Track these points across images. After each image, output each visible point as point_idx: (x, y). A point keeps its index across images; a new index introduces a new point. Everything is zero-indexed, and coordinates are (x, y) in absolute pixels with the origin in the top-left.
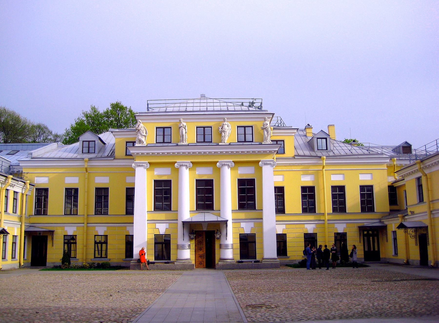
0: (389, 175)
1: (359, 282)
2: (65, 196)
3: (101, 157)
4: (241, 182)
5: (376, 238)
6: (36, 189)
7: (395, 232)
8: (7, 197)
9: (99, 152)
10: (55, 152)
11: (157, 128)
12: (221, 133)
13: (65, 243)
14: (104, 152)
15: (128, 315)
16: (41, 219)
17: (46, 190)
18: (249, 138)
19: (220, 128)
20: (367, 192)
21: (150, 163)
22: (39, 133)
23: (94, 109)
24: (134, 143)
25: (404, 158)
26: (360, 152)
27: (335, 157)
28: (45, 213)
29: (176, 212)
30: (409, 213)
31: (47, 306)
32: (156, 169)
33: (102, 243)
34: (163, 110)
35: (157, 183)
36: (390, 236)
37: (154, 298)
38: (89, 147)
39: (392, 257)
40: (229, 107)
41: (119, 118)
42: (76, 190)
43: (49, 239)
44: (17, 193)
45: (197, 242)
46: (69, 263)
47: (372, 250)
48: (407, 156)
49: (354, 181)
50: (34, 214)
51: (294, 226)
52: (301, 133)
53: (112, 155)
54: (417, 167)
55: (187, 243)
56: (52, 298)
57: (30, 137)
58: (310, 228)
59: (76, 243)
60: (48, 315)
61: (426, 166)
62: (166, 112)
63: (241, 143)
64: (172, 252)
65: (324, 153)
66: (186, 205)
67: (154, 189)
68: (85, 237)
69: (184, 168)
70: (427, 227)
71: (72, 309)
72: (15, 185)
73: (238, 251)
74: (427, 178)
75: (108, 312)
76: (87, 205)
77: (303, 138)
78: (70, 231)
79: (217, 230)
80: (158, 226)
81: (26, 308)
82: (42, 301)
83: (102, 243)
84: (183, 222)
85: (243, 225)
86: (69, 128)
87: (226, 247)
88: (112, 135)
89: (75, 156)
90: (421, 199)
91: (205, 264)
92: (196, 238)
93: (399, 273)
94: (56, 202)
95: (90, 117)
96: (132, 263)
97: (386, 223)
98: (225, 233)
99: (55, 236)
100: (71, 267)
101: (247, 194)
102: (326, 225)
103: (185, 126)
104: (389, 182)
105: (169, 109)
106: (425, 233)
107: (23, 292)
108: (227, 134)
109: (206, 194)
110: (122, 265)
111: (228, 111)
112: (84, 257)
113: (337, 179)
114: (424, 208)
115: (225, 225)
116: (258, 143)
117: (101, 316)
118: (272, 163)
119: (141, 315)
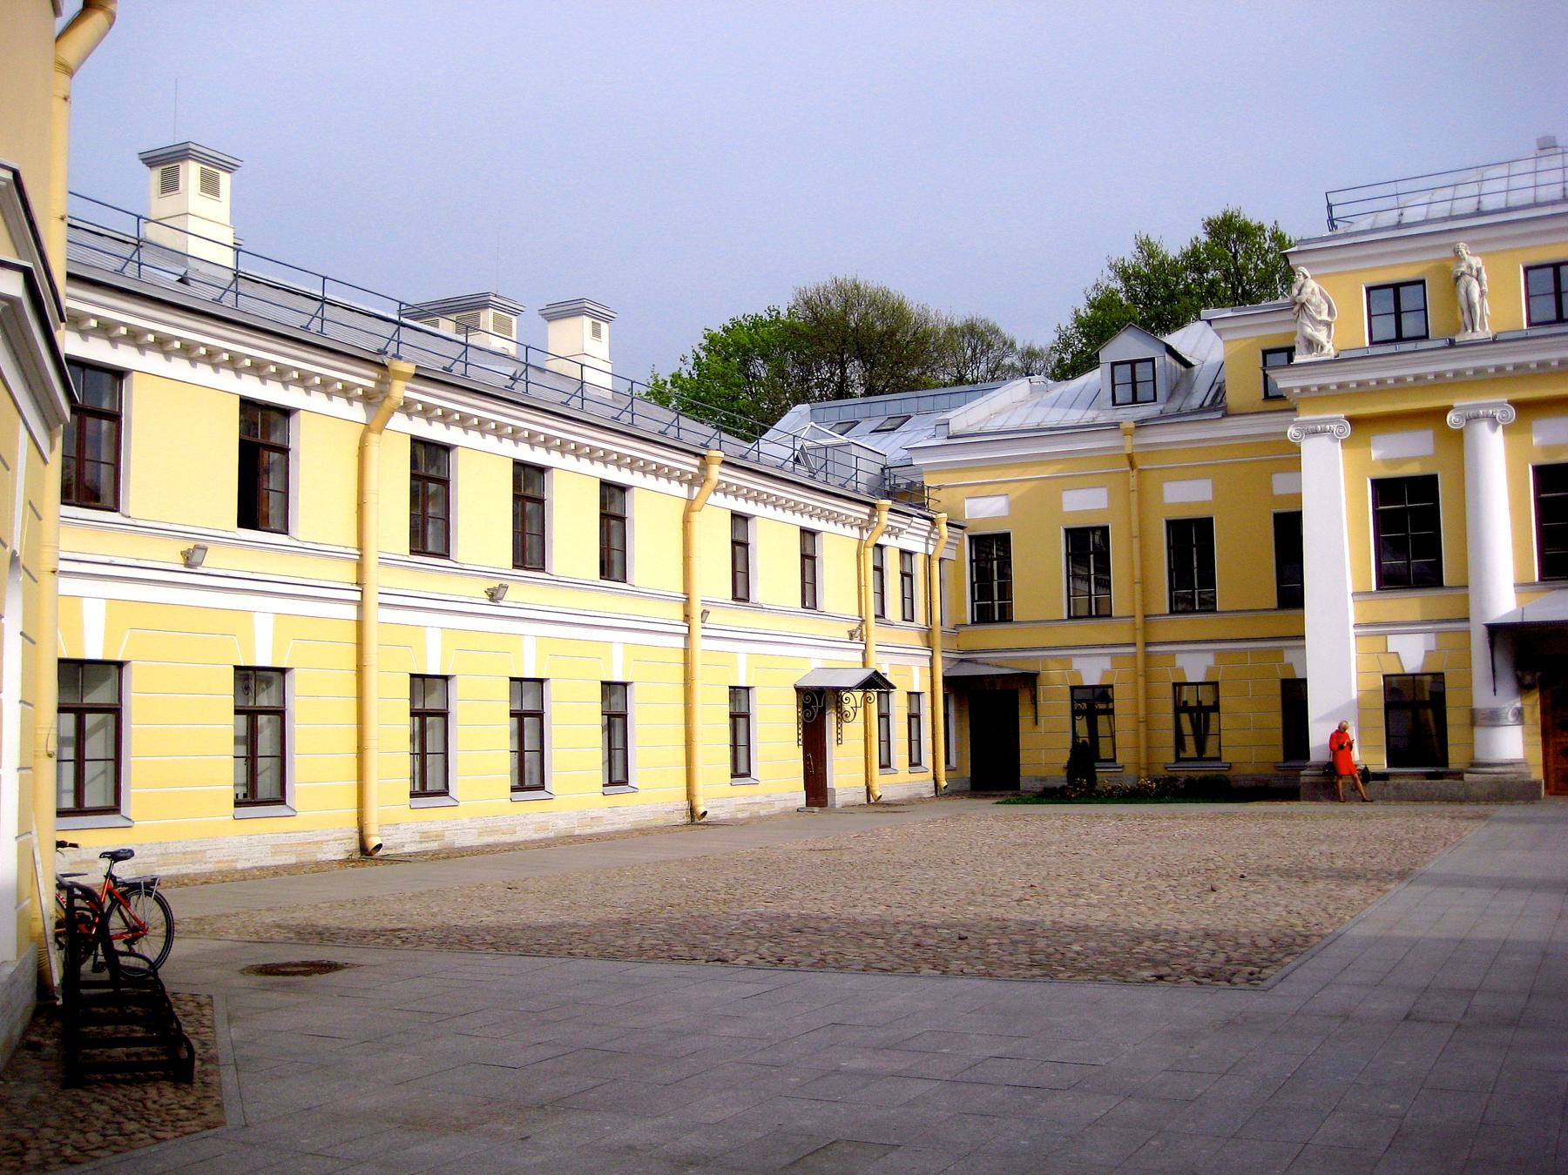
2: (1068, 555)
3: (1179, 413)
6: (971, 538)
8: (879, 570)
9: (1171, 395)
10: (1024, 411)
11: (1369, 290)
13: (1075, 713)
14: (1189, 393)
15: (1256, 959)
16: (994, 635)
17: (1004, 540)
21: (1353, 420)
22: (974, 351)
23: (1147, 248)
24: (1290, 351)
28: (1006, 617)
29: (1462, 592)
31: (997, 920)
34: (1390, 218)
35: (1384, 489)
37: (1365, 900)
38: (1134, 383)
41: (1237, 267)
44: (911, 554)
46: (1092, 779)
50: (969, 621)
53: (1217, 404)
55: (1509, 703)
56: (1018, 894)
57: (945, 366)
59: (1110, 712)
60: (994, 949)
62: (1399, 225)
64: (1454, 735)
69: (1484, 427)
71: (1073, 929)
72: (901, 530)
75: (1193, 943)
76: (1144, 582)
78: (1092, 671)
80: (1395, 643)
81: (930, 921)
82: (984, 903)
83: (1196, 713)
86: (1067, 322)
88: (1210, 333)
89: (1089, 416)
94: (1039, 575)
95: (1137, 276)
96: (1306, 776)
100: (1099, 794)
103: (1478, 271)
105: (1411, 215)
107: (931, 873)
110: (1275, 783)
112: (1143, 761)
117: (1162, 956)
119: (1304, 957)
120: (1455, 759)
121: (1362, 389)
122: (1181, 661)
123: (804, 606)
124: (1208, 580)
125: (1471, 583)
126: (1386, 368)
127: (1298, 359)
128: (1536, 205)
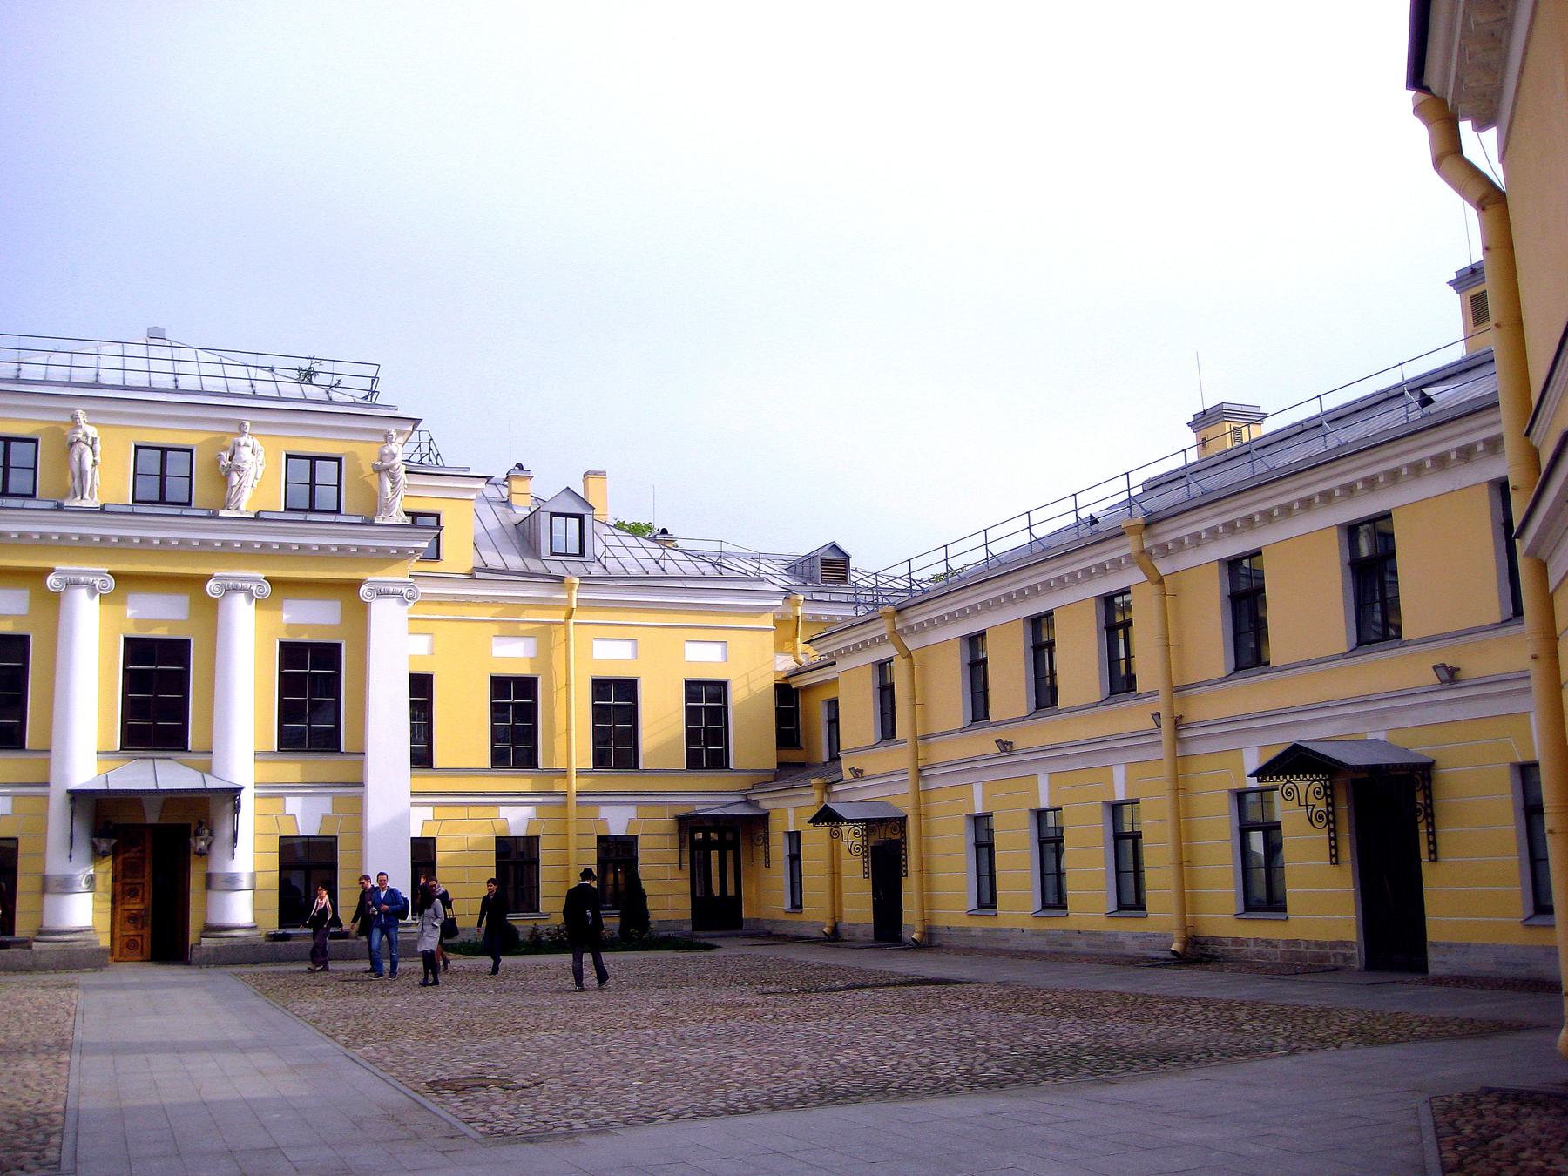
0: (779, 648)
1: (725, 996)
4: (137, 649)
5: (730, 855)
7: (794, 837)
12: (224, 476)
18: (326, 497)
19: (226, 455)
20: (707, 703)
25: (826, 597)
26: (690, 568)
27: (609, 581)
29: (45, 755)
30: (847, 775)
32: (287, 603)
36: (779, 848)
39: (783, 917)
40: (180, 378)
45: (120, 868)
47: (716, 892)
48: (840, 592)
49: (663, 662)
51: (461, 812)
52: (491, 492)
54: (883, 628)
55: (83, 871)
58: (516, 820)
61: (911, 627)
63: (300, 517)
65: (572, 567)
70: (902, 821)
73: (274, 900)
74: (912, 666)
77: (497, 508)
79: (201, 824)
84: (70, 792)
85: (294, 805)
87: (231, 883)
90: (888, 731)
91: (147, 946)
92: (115, 852)
93: (827, 966)
97: (766, 804)
98: (228, 833)
101: (313, 693)
102: (572, 811)
103: (94, 440)
104: (777, 672)
105: (29, 372)
106: (897, 837)
108: (249, 479)
109: (158, 689)
111: (97, 385)
113: (612, 656)
114: (897, 757)
115: (229, 806)
116: (204, 513)
118: (405, 591)
120: (22, 928)
121: (23, 541)
125: (53, 748)
126: (91, 525)
128: (201, 393)
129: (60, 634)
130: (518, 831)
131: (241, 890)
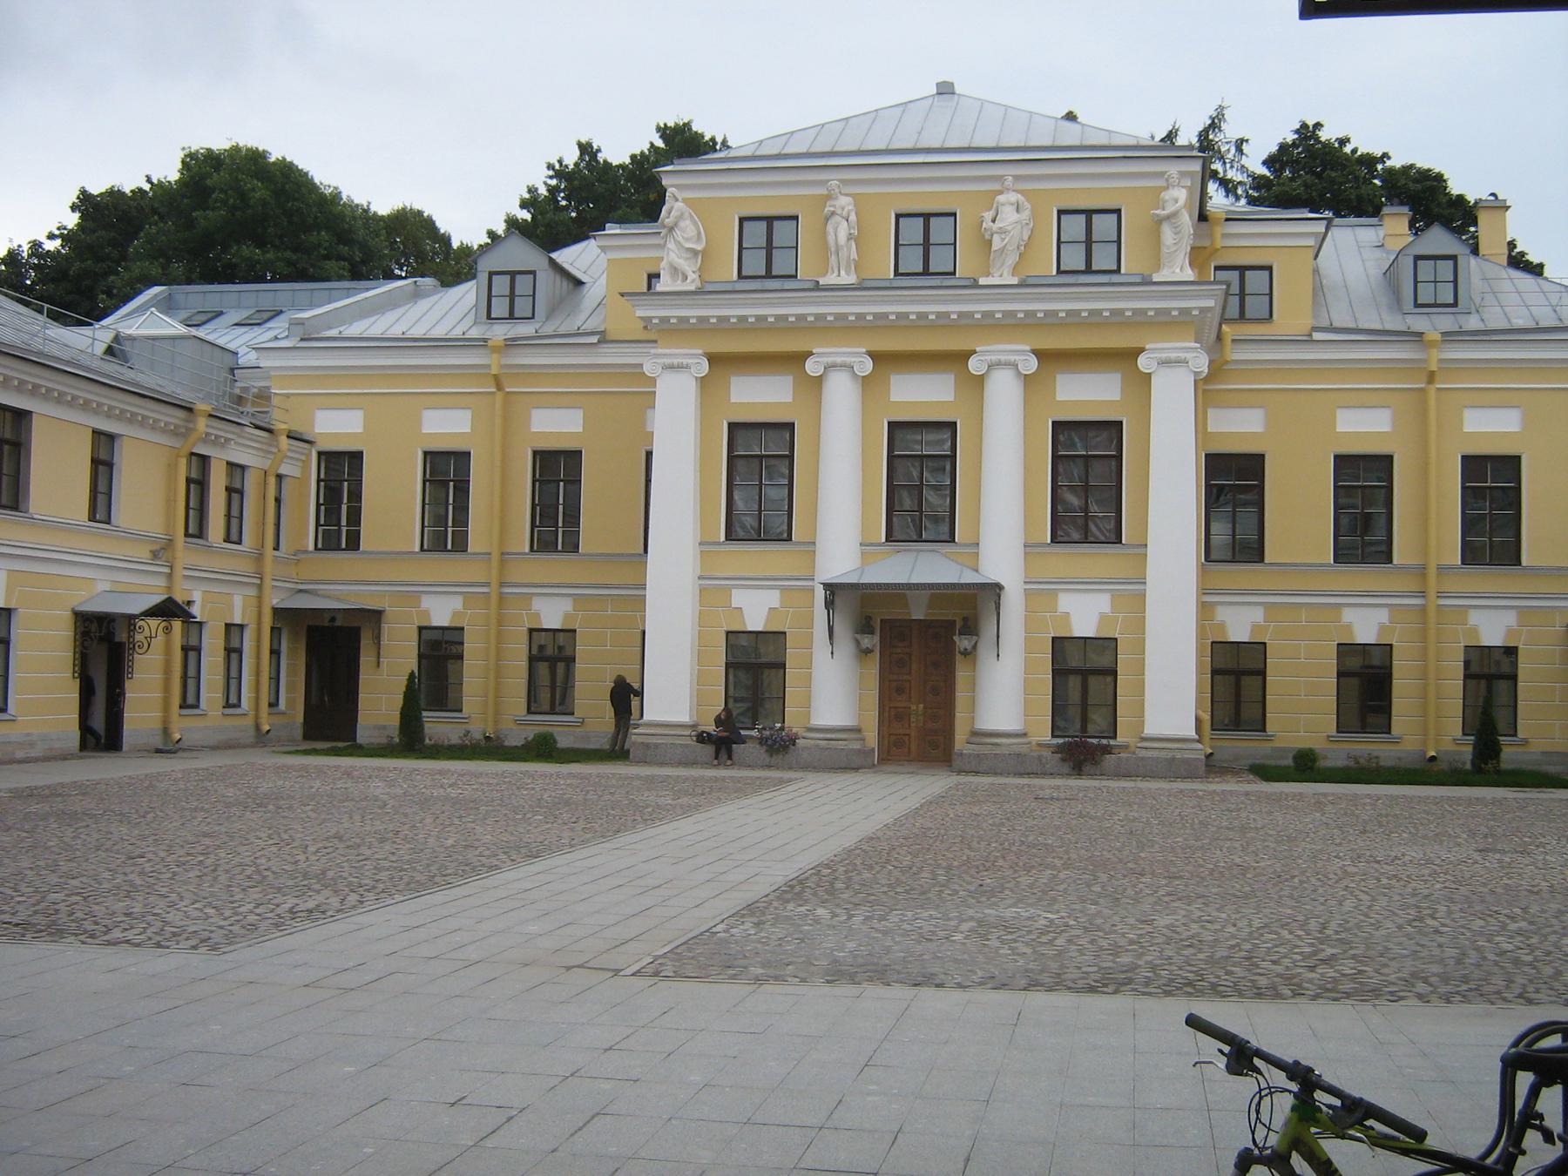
6: (320, 454)
16: (340, 564)
17: (356, 457)
33: (552, 658)
42: (463, 457)
43: (366, 643)
44: (243, 468)
50: (311, 547)
66: (842, 520)
67: (1463, 488)
68: (493, 632)
72: (227, 440)
78: (441, 612)
94: (393, 501)
99: (385, 627)
101: (1087, 482)
109: (921, 478)
116: (1138, 280)
122: (1474, 618)
123: (92, 518)
124: (573, 517)
126: (691, 306)
127: (659, 287)
129: (1022, 422)
130: (755, 623)
131: (1004, 694)
